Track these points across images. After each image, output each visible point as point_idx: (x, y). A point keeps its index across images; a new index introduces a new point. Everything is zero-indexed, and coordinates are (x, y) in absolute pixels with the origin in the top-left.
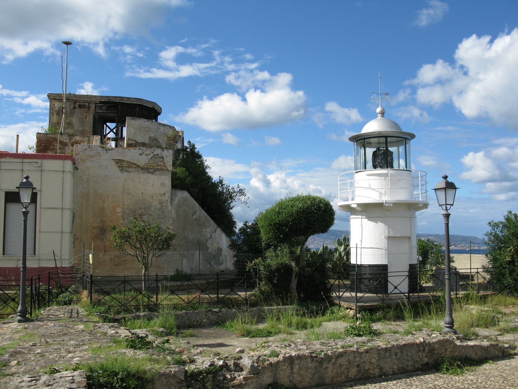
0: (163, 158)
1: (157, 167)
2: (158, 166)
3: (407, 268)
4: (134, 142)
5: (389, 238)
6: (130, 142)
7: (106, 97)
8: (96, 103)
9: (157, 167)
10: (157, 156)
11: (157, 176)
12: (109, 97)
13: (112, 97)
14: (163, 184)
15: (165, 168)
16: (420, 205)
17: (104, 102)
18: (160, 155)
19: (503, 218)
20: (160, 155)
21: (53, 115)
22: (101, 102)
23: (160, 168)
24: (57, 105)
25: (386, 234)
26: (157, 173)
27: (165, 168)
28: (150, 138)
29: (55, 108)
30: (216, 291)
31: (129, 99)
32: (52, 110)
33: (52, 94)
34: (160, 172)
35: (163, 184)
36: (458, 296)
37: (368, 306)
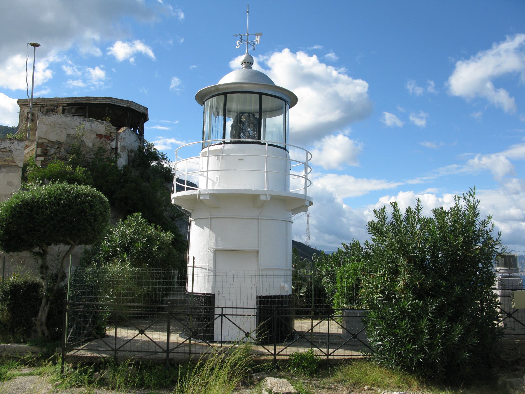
0: (12, 152)
1: (3, 163)
2: (5, 161)
3: (253, 303)
4: (46, 141)
5: (217, 252)
6: (40, 141)
7: (73, 98)
8: (63, 106)
9: (3, 163)
10: (4, 150)
11: (2, 174)
12: (76, 98)
13: (79, 98)
14: (10, 184)
15: (14, 164)
16: (263, 198)
17: (71, 103)
18: (8, 149)
19: (373, 214)
20: (8, 149)
21: (22, 122)
22: (69, 105)
23: (7, 163)
24: (26, 110)
25: (213, 245)
26: (4, 170)
27: (14, 164)
28: (68, 136)
29: (24, 114)
30: (171, 347)
31: (96, 98)
32: (22, 116)
33: (21, 100)
34: (7, 168)
35: (10, 184)
36: (277, 357)
37: (23, 347)
